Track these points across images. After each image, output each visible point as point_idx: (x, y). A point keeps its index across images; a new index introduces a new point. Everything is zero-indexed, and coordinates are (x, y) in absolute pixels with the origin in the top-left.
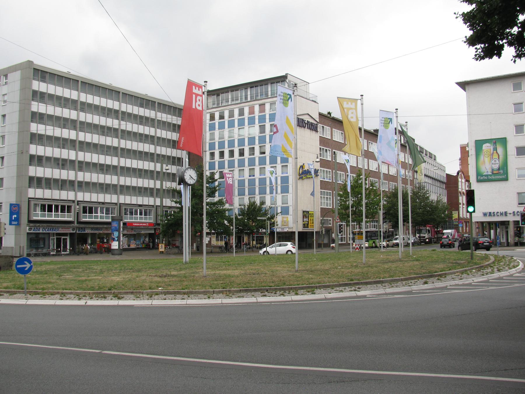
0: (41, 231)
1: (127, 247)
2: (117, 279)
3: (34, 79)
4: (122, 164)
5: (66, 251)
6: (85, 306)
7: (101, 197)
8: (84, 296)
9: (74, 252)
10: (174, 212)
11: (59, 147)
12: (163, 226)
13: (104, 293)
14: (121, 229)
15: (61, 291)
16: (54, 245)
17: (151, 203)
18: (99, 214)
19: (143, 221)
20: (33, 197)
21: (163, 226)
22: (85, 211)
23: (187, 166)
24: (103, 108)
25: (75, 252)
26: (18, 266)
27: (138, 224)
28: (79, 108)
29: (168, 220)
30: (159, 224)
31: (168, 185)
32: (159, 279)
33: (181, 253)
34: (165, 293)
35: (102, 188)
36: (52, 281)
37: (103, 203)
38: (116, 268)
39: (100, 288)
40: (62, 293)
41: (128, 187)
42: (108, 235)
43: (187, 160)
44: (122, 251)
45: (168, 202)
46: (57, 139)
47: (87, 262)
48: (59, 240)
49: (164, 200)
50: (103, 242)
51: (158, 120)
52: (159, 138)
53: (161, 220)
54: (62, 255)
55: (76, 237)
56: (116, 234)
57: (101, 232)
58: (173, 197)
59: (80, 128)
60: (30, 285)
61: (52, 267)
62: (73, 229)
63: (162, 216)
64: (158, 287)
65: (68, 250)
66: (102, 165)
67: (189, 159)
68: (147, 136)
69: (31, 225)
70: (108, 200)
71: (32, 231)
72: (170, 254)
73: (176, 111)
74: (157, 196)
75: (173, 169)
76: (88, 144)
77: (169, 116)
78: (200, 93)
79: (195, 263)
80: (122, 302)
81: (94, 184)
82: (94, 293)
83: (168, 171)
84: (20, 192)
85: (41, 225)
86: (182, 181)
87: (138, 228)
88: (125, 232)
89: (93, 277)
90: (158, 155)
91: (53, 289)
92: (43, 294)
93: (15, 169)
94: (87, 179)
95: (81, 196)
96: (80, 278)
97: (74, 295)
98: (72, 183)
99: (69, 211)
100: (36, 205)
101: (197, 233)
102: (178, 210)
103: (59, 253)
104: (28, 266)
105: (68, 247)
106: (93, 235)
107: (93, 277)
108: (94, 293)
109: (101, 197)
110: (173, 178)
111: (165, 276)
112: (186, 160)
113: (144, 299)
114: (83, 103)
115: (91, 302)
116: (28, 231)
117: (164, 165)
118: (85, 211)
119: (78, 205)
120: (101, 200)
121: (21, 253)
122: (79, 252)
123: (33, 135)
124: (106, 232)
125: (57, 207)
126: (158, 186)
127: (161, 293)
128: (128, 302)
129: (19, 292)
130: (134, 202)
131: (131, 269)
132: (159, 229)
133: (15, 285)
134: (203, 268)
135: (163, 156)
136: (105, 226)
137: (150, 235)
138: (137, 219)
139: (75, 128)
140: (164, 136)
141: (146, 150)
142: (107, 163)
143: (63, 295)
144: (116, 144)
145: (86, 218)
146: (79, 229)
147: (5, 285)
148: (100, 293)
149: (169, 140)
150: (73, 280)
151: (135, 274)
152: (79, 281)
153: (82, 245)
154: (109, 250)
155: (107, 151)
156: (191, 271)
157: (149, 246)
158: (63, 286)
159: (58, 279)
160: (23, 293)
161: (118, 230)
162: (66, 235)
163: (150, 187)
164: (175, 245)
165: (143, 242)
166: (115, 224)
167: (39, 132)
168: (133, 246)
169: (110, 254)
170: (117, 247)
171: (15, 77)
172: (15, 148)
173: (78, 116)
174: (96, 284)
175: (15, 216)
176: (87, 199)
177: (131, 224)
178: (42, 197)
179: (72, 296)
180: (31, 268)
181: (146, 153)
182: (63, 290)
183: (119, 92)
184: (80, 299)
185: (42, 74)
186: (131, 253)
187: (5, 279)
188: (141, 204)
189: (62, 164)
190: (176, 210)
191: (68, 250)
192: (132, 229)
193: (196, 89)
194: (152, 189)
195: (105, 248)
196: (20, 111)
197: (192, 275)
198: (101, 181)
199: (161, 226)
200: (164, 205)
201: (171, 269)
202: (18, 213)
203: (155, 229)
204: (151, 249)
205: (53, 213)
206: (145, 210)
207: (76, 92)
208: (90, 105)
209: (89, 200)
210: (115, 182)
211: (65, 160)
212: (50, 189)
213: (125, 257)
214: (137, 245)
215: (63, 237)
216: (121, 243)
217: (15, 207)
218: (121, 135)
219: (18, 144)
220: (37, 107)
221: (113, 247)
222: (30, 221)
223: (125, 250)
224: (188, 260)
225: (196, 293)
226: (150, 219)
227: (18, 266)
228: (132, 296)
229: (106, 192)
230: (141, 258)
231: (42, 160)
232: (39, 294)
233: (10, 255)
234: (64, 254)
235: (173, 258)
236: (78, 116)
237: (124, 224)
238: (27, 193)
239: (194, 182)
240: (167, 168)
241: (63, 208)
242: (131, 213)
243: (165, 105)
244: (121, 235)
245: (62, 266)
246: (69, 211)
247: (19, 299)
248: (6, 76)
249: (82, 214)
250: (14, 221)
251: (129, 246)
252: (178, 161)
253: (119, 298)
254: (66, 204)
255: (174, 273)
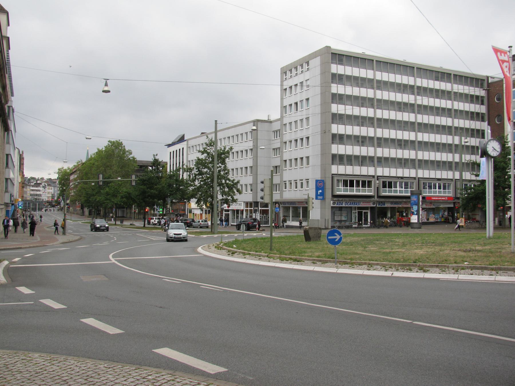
0: (344, 205)
1: (426, 221)
2: (420, 252)
3: (332, 63)
4: (420, 139)
5: (367, 224)
6: (391, 277)
7: (400, 172)
8: (390, 267)
9: (374, 225)
10: (474, 185)
11: (358, 125)
12: (463, 199)
13: (409, 265)
14: (420, 203)
15: (367, 262)
16: (355, 218)
17: (450, 177)
18: (398, 189)
19: (437, 195)
20: (336, 173)
21: (463, 199)
22: (384, 186)
23: (490, 138)
24: (399, 85)
25: (375, 225)
26: (329, 238)
27: (437, 198)
28: (375, 86)
29: (469, 194)
30: (458, 198)
31: (467, 158)
32: (462, 254)
33: (483, 226)
34: (472, 268)
35: (401, 163)
36: (359, 252)
37: (402, 178)
38: (418, 241)
39: (405, 261)
40: (369, 264)
41: (426, 162)
42: (407, 209)
43: (489, 131)
44: (421, 224)
45: (468, 176)
46: (356, 117)
47: (388, 235)
48: (360, 214)
49: (464, 173)
50: (402, 216)
51: (455, 93)
52: (456, 111)
53: (461, 194)
54: (363, 228)
55: (377, 210)
56: (415, 208)
57: (400, 206)
58: (473, 169)
59: (377, 105)
60: (338, 255)
61: (356, 239)
62: (374, 203)
63: (462, 190)
64: (464, 261)
65: (369, 223)
66: (399, 141)
67: (491, 130)
68: (443, 109)
69: (335, 199)
70: (406, 175)
71: (335, 205)
72: (470, 228)
73: (473, 82)
74: (456, 170)
75: (474, 142)
76: (386, 121)
77: (466, 88)
78: (506, 58)
79: (499, 238)
80: (427, 275)
81: (393, 159)
82: (399, 265)
83: (467, 144)
84: (324, 169)
85: (343, 199)
86: (484, 153)
87: (437, 202)
88: (424, 206)
89: (396, 249)
90: (456, 128)
91: (360, 260)
92: (352, 264)
93: (319, 148)
94: (386, 155)
95: (380, 171)
96: (384, 251)
97: (381, 266)
98: (371, 159)
99: (369, 186)
100: (338, 181)
101: (499, 206)
102: (479, 183)
103: (361, 226)
104: (338, 237)
105: (369, 220)
106: (393, 209)
107: (396, 249)
108: (399, 265)
109: (400, 172)
110: (472, 151)
111: (470, 251)
112: (488, 131)
113: (449, 273)
114: (379, 82)
115: (397, 274)
116: (332, 205)
117: (463, 138)
118: (384, 186)
119: (378, 180)
120: (400, 174)
121: (326, 226)
122: (379, 225)
123: (334, 115)
124: (405, 206)
125: (358, 182)
126: (457, 159)
127: (468, 268)
128: (433, 275)
129: (330, 261)
130: (432, 176)
131: (433, 243)
132: (459, 203)
133: (325, 254)
134: (510, 244)
135: (462, 129)
136: (404, 200)
137: (449, 209)
138: (436, 193)
139: (372, 106)
140: (461, 108)
141: (444, 123)
142: (404, 138)
143: (370, 266)
144: (412, 119)
145: (386, 192)
146: (379, 203)
147: (317, 254)
148: (405, 265)
149: (467, 112)
150: (378, 252)
151: (437, 248)
152: (384, 253)
153: (382, 218)
154: (408, 224)
155: (404, 127)
156: (497, 247)
157: (448, 219)
158: (369, 257)
159: (363, 250)
160: (334, 262)
161: (418, 204)
162: (366, 208)
163: (449, 160)
164: (475, 219)
165: (442, 217)
166: (414, 199)
167: (339, 112)
168: (432, 220)
169: (409, 228)
170: (416, 221)
171: (316, 63)
172: (319, 129)
173: (375, 94)
174: (400, 256)
175: (321, 191)
176: (386, 174)
177: (430, 198)
178: (344, 173)
179: (379, 267)
180: (340, 239)
181: (444, 127)
182: (370, 261)
183: (414, 67)
184: (386, 270)
185: (339, 57)
186: (430, 227)
187: (315, 248)
188: (440, 177)
189: (362, 141)
190: (476, 184)
191: (369, 223)
192: (431, 203)
193: (501, 55)
194: (450, 163)
195: (404, 221)
196: (321, 93)
197: (499, 250)
198: (400, 156)
199: (461, 199)
200: (464, 178)
201: (474, 243)
202: (323, 189)
203: (454, 203)
204: (450, 223)
205: (355, 188)
206: (444, 184)
207: (372, 72)
208: (386, 83)
209: (388, 175)
210: (413, 157)
211: (364, 138)
212: (351, 165)
213: (424, 230)
214: (436, 219)
215: (364, 211)
216: (420, 217)
217: (320, 182)
218: (418, 110)
219: (321, 124)
220: (337, 89)
221: (412, 221)
222: (334, 196)
223: (424, 224)
224: (491, 235)
225: (506, 270)
226: (449, 193)
227: (329, 238)
228: (437, 269)
229: (405, 167)
230: (441, 232)
231: (343, 138)
232: (347, 264)
233: (316, 226)
234: (365, 227)
235: (474, 233)
236: (375, 94)
237: (423, 198)
238: (330, 169)
239: (498, 153)
240: (466, 140)
241: (364, 183)
242: (430, 187)
243: (461, 76)
244: (421, 209)
245: (365, 238)
246: (369, 186)
247: (331, 267)
248: (308, 63)
249: (381, 189)
250: (320, 195)
251: (428, 219)
252: (480, 134)
253: (425, 271)
254: (367, 180)
255: (478, 248)
